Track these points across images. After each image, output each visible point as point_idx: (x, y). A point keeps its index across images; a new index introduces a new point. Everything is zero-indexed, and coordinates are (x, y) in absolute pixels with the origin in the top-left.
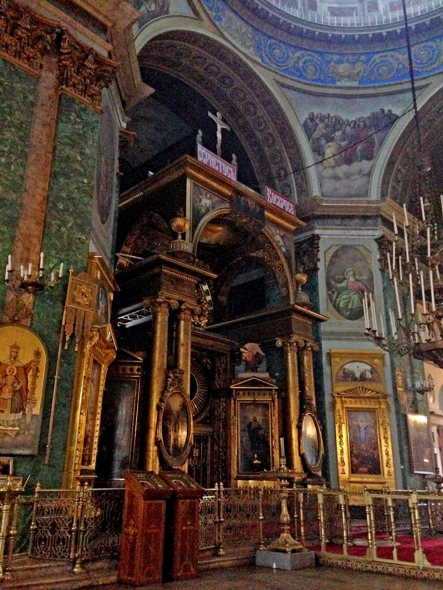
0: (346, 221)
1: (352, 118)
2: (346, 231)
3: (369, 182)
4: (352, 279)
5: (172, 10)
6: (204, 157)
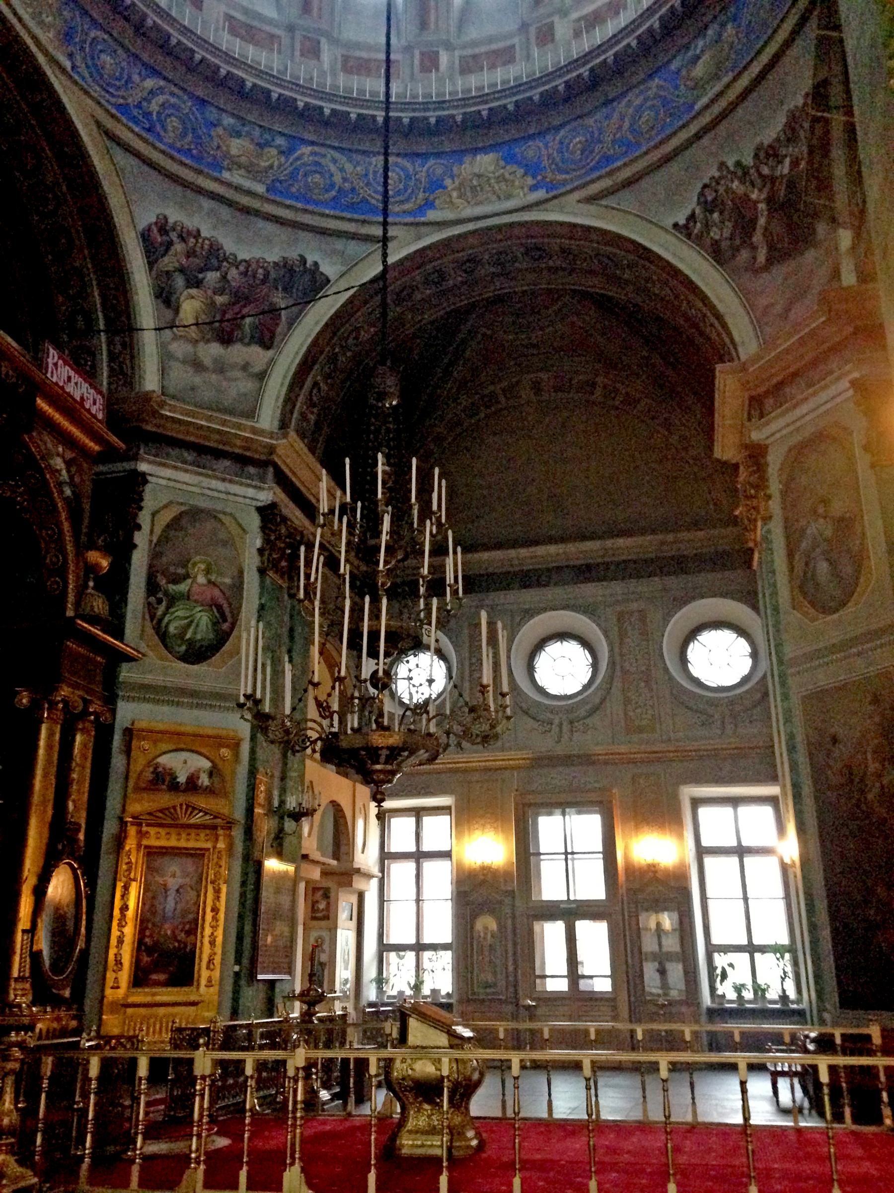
0: (206, 459)
1: (243, 255)
3: (259, 393)
4: (201, 579)
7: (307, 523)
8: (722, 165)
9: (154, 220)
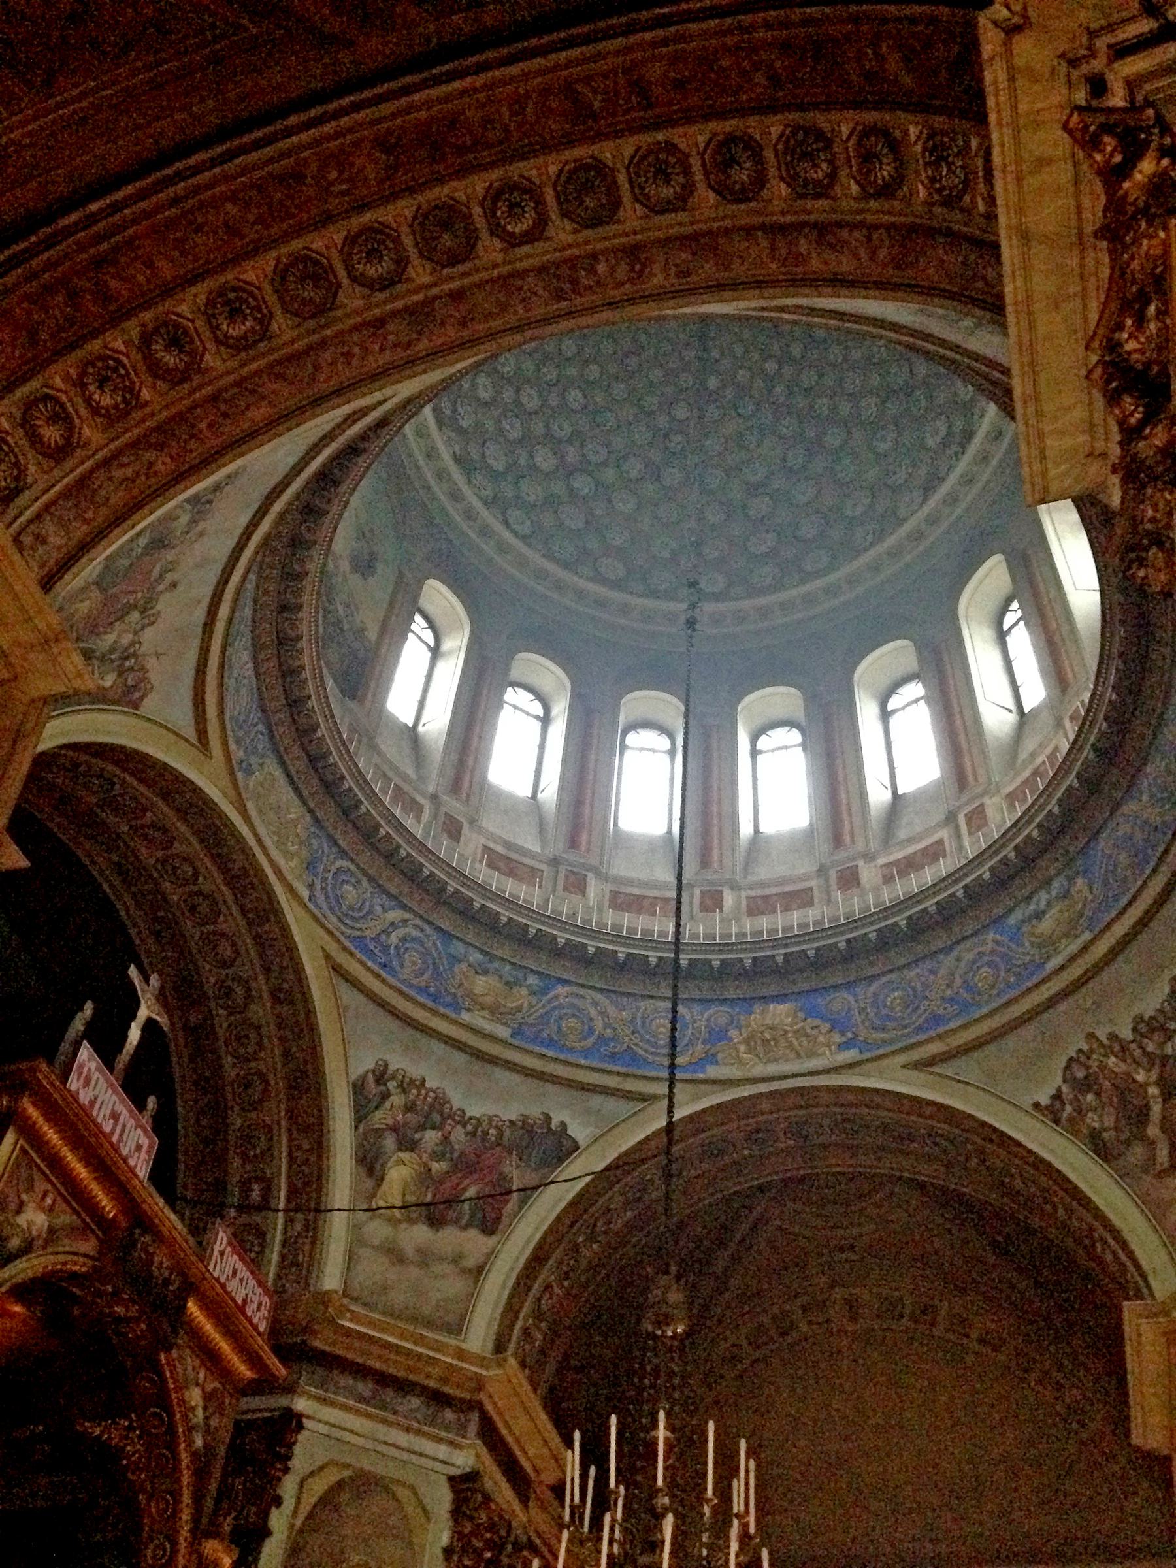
1: (473, 1111)
2: (380, 1426)
3: (471, 1297)
5: (150, 705)
6: (87, 1083)
7: (517, 1506)
8: (1091, 1036)
9: (372, 1066)
